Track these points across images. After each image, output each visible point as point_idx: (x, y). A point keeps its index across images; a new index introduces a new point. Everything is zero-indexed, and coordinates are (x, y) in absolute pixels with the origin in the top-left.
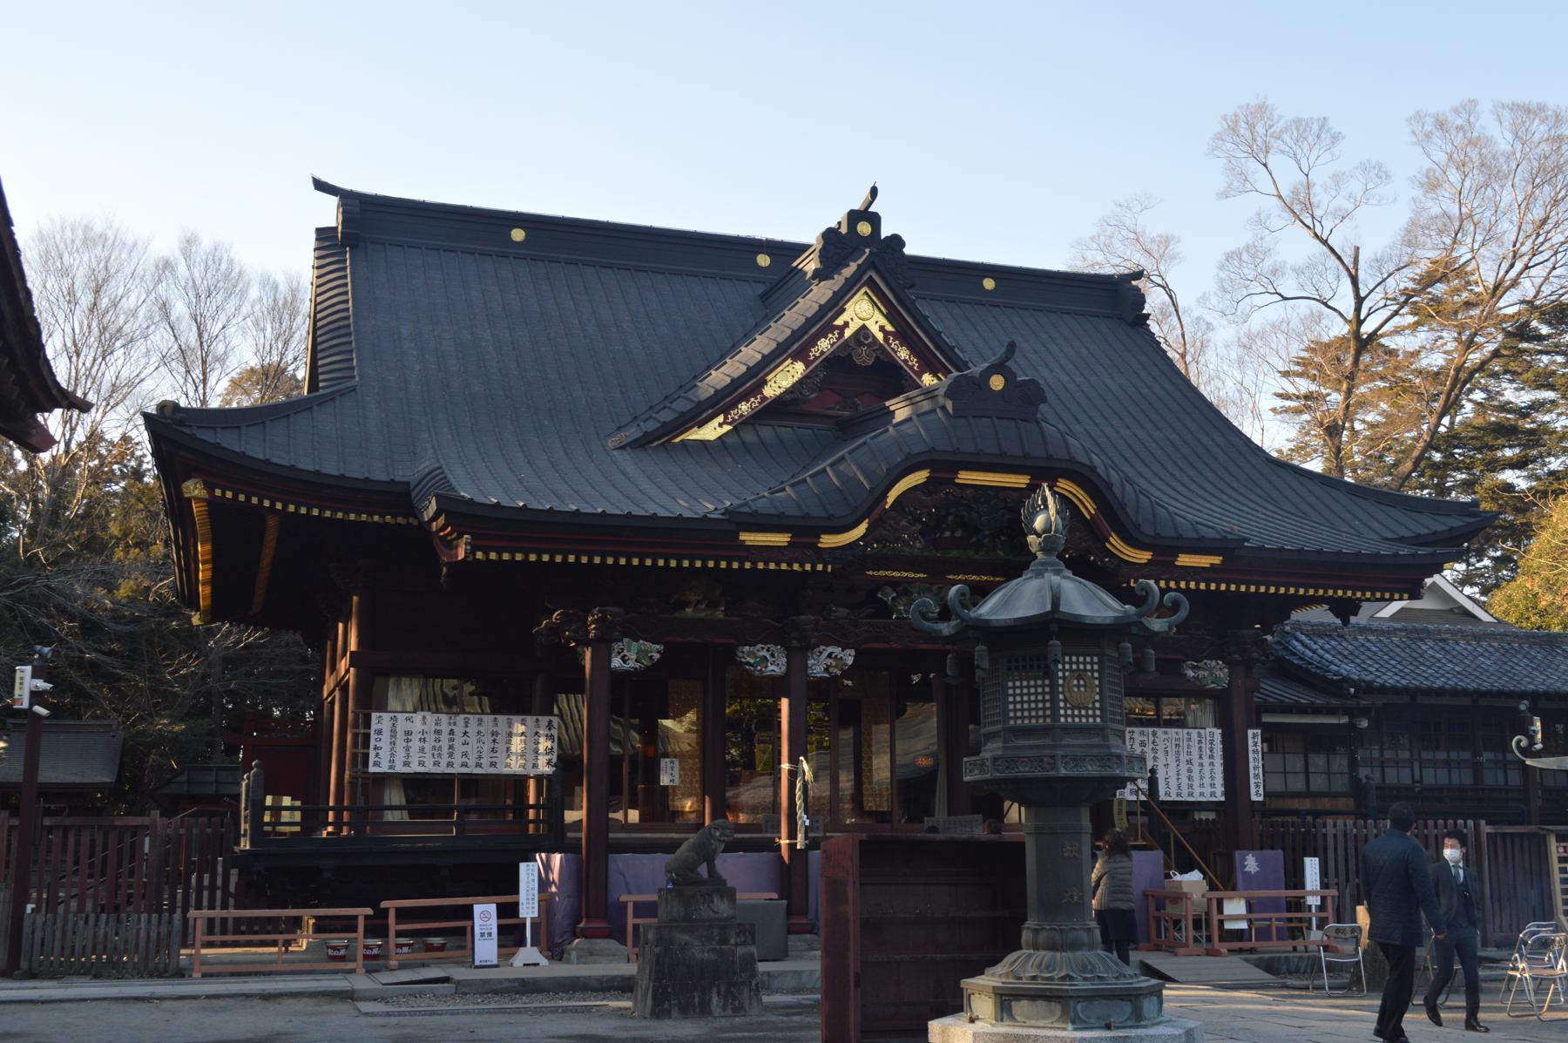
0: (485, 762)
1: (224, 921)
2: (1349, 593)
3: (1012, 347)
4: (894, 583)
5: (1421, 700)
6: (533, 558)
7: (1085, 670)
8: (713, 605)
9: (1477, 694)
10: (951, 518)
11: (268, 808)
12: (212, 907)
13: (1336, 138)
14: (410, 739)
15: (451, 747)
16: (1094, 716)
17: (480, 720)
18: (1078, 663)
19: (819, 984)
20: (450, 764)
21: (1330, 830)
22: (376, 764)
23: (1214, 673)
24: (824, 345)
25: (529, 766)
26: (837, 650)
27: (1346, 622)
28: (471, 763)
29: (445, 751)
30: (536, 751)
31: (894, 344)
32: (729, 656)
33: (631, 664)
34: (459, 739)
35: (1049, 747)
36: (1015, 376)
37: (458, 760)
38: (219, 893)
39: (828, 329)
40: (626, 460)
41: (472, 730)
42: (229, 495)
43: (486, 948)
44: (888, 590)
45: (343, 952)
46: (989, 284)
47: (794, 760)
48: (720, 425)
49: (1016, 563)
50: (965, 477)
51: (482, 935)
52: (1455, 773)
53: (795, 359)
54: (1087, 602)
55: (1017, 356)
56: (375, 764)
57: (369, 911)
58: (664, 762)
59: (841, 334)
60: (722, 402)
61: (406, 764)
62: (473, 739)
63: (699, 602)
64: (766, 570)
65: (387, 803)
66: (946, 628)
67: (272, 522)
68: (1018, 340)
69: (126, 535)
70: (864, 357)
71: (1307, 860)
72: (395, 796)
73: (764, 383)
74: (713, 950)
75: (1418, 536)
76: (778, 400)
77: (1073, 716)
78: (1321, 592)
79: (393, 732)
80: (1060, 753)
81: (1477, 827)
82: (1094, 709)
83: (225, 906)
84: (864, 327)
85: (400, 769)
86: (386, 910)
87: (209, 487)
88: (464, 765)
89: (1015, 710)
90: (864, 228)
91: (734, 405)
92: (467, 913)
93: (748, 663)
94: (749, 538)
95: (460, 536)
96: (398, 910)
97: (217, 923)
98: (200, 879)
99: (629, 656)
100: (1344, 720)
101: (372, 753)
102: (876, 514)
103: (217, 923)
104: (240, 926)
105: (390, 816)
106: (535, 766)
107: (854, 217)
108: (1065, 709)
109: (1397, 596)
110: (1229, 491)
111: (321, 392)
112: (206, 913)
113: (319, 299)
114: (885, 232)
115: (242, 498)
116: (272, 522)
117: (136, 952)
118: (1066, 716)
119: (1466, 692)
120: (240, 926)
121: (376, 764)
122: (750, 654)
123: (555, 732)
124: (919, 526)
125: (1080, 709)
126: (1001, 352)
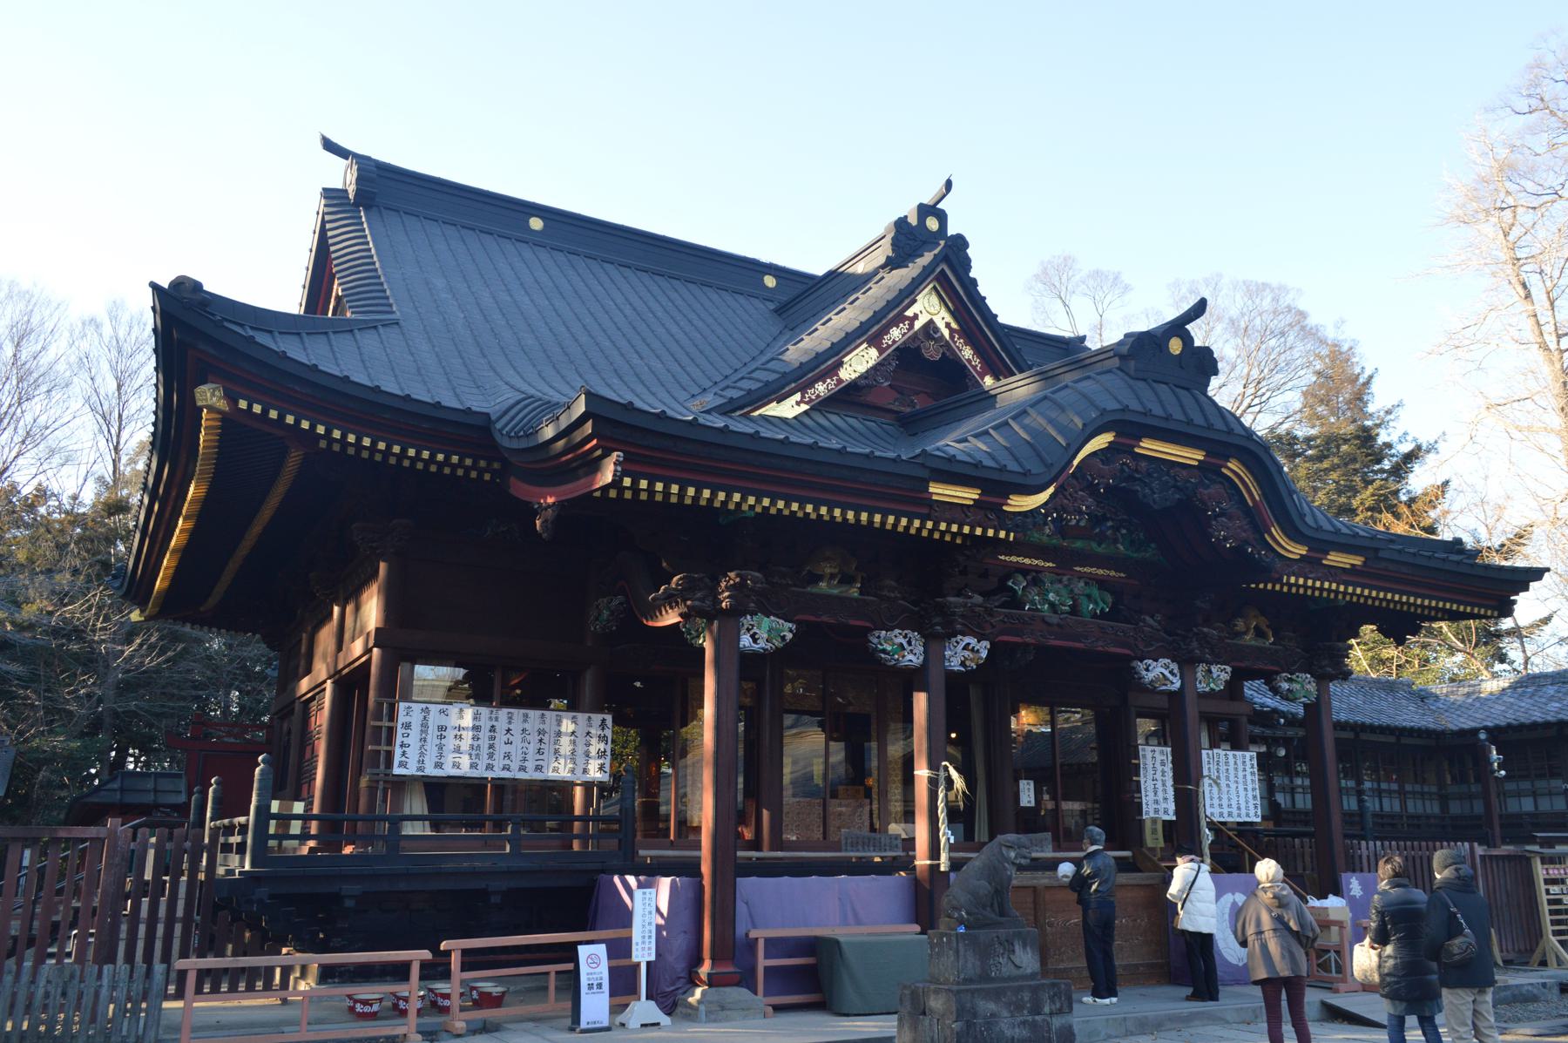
0: (530, 765)
4: (1024, 571)
8: (846, 580)
11: (274, 816)
13: (1127, 288)
14: (446, 734)
15: (491, 746)
17: (526, 716)
20: (490, 767)
21: (1365, 853)
22: (403, 765)
24: (896, 334)
25: (579, 771)
26: (973, 641)
28: (515, 765)
29: (485, 751)
30: (587, 755)
31: (960, 342)
33: (762, 644)
34: (501, 737)
37: (499, 762)
39: (899, 319)
41: (516, 727)
43: (595, 1006)
44: (1020, 578)
45: (375, 1008)
47: (933, 765)
48: (798, 403)
50: (1150, 447)
51: (590, 986)
52: (1386, 802)
56: (402, 764)
57: (426, 954)
59: (911, 326)
60: (799, 379)
61: (439, 765)
62: (517, 738)
63: (832, 576)
65: (407, 812)
69: (31, 561)
70: (932, 352)
72: (416, 804)
73: (840, 364)
74: (1024, 1023)
76: (854, 386)
79: (424, 726)
81: (1472, 849)
84: (931, 322)
85: (430, 771)
86: (448, 953)
87: (232, 398)
88: (506, 768)
91: (811, 384)
92: (568, 953)
93: (884, 651)
95: (606, 454)
96: (465, 952)
101: (398, 751)
102: (1061, 479)
105: (409, 829)
106: (585, 771)
107: (925, 210)
113: (328, 226)
117: (78, 1008)
121: (403, 765)
122: (887, 640)
123: (608, 733)
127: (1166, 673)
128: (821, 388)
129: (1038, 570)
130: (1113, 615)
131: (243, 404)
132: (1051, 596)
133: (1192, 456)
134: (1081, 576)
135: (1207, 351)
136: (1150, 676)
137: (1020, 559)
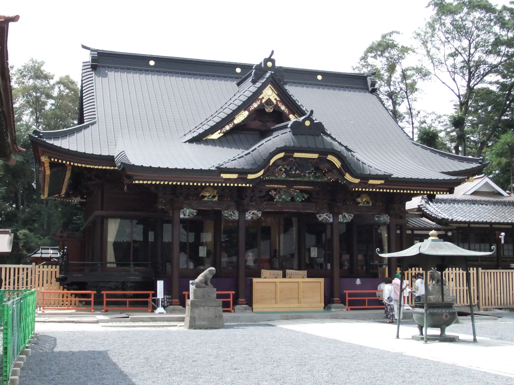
4: (275, 189)
5: (472, 225)
26: (255, 212)
33: (187, 217)
42: (56, 160)
44: (273, 191)
46: (319, 77)
48: (219, 133)
50: (296, 155)
53: (245, 110)
58: (201, 248)
59: (261, 101)
63: (209, 196)
67: (69, 168)
70: (269, 109)
71: (158, 282)
84: (269, 99)
87: (50, 158)
99: (187, 213)
105: (109, 265)
107: (266, 60)
110: (385, 159)
111: (85, 124)
113: (84, 78)
122: (226, 213)
127: (327, 217)
128: (227, 128)
129: (281, 189)
130: (307, 200)
131: (53, 159)
133: (315, 156)
136: (320, 219)
137: (273, 186)
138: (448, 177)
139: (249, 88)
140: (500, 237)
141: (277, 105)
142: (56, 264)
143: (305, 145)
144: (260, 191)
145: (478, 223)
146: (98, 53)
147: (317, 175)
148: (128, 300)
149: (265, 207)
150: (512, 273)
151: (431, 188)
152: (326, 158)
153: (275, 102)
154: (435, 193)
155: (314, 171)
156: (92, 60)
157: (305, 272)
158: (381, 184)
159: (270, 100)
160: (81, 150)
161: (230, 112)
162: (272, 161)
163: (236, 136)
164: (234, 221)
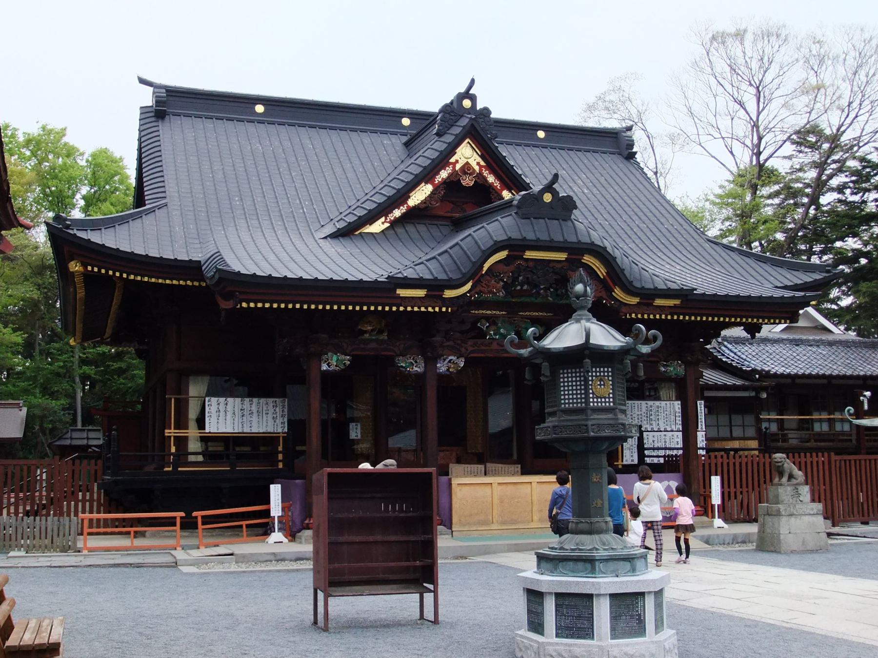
1: (98, 520)
2: (755, 320)
3: (556, 176)
4: (487, 318)
5: (798, 381)
6: (275, 306)
7: (604, 376)
9: (831, 377)
10: (521, 278)
12: (91, 512)
16: (609, 402)
18: (600, 372)
19: (312, 555)
23: (675, 369)
24: (444, 174)
27: (753, 337)
32: (390, 361)
33: (332, 368)
35: (584, 420)
36: (558, 193)
38: (95, 503)
40: (327, 245)
42: (96, 269)
44: (483, 321)
48: (383, 223)
49: (563, 314)
50: (529, 254)
53: (426, 183)
54: (605, 337)
55: (560, 180)
57: (183, 514)
58: (352, 426)
59: (454, 167)
63: (372, 330)
64: (412, 311)
66: (524, 352)
67: (119, 284)
68: (562, 173)
70: (467, 181)
71: (272, 487)
75: (796, 285)
76: (415, 208)
77: (597, 402)
78: (739, 320)
80: (590, 423)
82: (609, 398)
83: (99, 512)
84: (467, 163)
87: (85, 266)
89: (565, 399)
90: (467, 103)
93: (402, 367)
94: (402, 293)
97: (95, 521)
98: (84, 496)
99: (332, 362)
100: (753, 394)
103: (95, 521)
104: (115, 523)
108: (593, 398)
109: (783, 321)
112: (87, 515)
113: (143, 133)
114: (479, 106)
115: (103, 271)
116: (119, 284)
118: (593, 402)
119: (824, 376)
120: (115, 523)
124: (502, 283)
125: (601, 398)
126: (550, 178)
128: (397, 213)
129: (497, 317)
131: (89, 268)
132: (502, 331)
134: (523, 317)
135: (569, 197)
137: (484, 312)
138: (788, 294)
139: (430, 148)
140: (861, 398)
141: (480, 174)
142: (97, 456)
143: (544, 237)
144: (463, 322)
145: (810, 376)
146: (167, 91)
147: (559, 292)
148: (244, 523)
149: (470, 349)
150: (875, 460)
151: (752, 312)
152: (580, 260)
153: (477, 168)
154: (761, 321)
155: (554, 286)
156: (156, 102)
157: (518, 467)
158: (675, 306)
159: (471, 169)
160: (140, 251)
161: (400, 185)
162: (486, 266)
163: (411, 228)
164: (417, 375)
